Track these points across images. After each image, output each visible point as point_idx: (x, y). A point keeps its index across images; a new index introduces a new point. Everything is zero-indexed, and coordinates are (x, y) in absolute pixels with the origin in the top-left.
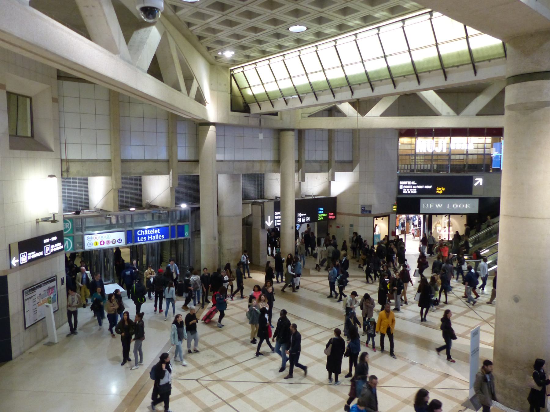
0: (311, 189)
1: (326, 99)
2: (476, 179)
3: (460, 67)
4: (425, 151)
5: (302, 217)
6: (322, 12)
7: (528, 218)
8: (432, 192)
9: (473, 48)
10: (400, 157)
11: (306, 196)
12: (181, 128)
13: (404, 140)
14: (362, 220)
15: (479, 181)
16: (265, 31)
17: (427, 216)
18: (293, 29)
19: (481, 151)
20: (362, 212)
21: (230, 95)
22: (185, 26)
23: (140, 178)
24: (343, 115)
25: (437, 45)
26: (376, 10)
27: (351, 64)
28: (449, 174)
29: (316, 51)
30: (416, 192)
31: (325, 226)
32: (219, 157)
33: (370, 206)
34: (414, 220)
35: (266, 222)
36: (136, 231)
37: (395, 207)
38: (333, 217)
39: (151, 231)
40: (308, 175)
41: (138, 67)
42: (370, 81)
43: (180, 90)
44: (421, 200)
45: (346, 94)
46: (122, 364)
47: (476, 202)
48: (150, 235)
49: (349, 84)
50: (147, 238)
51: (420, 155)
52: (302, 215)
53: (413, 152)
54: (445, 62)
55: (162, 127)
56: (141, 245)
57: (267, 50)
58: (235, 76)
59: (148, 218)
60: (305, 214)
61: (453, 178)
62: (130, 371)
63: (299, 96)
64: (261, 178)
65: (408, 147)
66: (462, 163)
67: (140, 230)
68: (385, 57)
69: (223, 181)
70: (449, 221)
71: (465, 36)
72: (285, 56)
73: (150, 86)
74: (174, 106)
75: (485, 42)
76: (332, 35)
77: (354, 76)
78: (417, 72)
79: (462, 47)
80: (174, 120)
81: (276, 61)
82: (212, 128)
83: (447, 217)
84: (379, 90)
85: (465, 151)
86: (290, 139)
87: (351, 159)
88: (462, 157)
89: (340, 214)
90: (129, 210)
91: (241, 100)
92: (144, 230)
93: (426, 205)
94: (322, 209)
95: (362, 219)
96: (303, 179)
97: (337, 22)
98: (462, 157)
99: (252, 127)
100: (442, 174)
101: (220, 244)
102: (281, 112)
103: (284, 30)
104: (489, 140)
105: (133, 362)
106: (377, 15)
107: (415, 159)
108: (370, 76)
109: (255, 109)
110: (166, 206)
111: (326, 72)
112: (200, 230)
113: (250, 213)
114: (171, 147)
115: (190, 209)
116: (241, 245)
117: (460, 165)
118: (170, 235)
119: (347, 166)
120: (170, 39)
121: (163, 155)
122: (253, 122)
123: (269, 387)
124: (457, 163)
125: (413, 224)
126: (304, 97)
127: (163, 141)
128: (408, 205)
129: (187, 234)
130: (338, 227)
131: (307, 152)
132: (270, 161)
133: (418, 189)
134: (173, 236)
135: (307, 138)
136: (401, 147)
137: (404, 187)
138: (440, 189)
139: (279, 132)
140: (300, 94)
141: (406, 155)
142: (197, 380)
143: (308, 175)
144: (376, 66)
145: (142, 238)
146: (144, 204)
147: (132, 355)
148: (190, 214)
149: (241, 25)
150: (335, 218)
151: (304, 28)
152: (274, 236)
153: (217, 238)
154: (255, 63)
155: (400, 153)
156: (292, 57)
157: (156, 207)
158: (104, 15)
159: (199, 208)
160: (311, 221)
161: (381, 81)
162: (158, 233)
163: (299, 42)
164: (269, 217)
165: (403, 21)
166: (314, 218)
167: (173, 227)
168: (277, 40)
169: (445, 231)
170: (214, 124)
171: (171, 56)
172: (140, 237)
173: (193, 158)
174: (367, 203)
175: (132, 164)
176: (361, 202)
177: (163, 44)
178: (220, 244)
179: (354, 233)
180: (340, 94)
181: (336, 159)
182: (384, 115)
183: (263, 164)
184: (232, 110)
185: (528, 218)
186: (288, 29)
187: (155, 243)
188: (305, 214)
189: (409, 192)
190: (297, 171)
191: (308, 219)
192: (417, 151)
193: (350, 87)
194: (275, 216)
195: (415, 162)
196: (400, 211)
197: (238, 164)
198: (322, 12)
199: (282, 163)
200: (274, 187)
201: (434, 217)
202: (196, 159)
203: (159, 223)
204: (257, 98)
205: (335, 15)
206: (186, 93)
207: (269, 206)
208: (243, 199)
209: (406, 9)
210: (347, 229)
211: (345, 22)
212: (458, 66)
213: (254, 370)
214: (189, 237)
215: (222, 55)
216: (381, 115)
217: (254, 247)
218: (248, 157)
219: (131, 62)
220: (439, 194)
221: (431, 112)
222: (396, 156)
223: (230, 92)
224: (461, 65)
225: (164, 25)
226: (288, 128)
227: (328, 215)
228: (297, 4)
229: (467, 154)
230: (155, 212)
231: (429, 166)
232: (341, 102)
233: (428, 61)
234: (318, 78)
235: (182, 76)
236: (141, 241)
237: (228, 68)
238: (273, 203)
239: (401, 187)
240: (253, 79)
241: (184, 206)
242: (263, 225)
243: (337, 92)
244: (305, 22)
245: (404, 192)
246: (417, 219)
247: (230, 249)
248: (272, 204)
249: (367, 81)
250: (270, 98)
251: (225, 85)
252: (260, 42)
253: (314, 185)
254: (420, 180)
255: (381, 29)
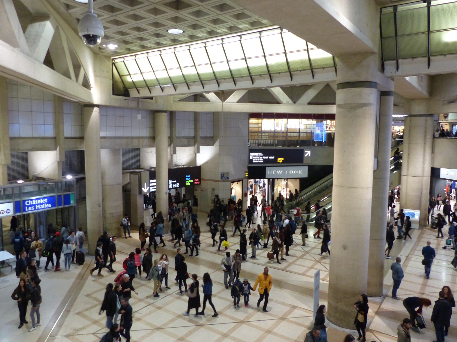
0: (180, 160)
1: (195, 89)
2: (306, 152)
3: (302, 72)
4: (269, 130)
5: (173, 183)
6: (198, 21)
7: (352, 187)
8: (274, 161)
9: (312, 58)
10: (250, 134)
11: (176, 165)
12: (67, 109)
13: (253, 121)
14: (222, 184)
15: (308, 153)
16: (147, 31)
17: (271, 180)
18: (171, 31)
19: (309, 130)
20: (222, 178)
21: (111, 81)
22: (75, 21)
23: (26, 154)
24: (207, 100)
25: (285, 53)
26: (240, 23)
27: (218, 63)
28: (285, 147)
29: (189, 50)
30: (262, 162)
31: (191, 189)
32: (103, 134)
33: (228, 173)
34: (260, 183)
35: (143, 189)
36: (24, 201)
37: (247, 173)
38: (198, 183)
39: (39, 201)
40: (178, 149)
41: (35, 59)
42: (233, 77)
43: (69, 77)
44: (267, 168)
45: (214, 87)
46: (20, 327)
47: (306, 168)
48: (38, 204)
49: (217, 79)
50: (35, 207)
51: (265, 132)
52: (173, 181)
53: (260, 130)
54: (291, 67)
55: (49, 108)
56: (28, 215)
57: (147, 45)
58: (116, 64)
59: (35, 189)
60: (176, 181)
61: (288, 150)
62: (28, 333)
63: (173, 85)
64: (137, 152)
65: (256, 126)
66: (295, 139)
67: (28, 200)
68: (245, 59)
69: (105, 156)
70: (287, 183)
71: (306, 48)
72: (162, 51)
73: (45, 76)
74: (66, 92)
75: (320, 55)
76: (203, 38)
77: (220, 72)
78: (270, 73)
79: (303, 56)
80: (59, 101)
81: (154, 55)
82: (96, 109)
83: (286, 180)
84: (240, 84)
85: (298, 130)
86: (164, 119)
87: (212, 136)
88: (295, 134)
89: (204, 180)
90: (17, 183)
91: (121, 85)
92: (32, 200)
93: (271, 172)
94: (189, 176)
95: (222, 184)
96: (174, 152)
97: (208, 29)
98: (295, 134)
99: (131, 109)
100: (280, 147)
101: (104, 211)
102: (156, 97)
103: (164, 32)
104: (314, 121)
105: (30, 324)
106: (240, 26)
107: (261, 136)
108: (233, 73)
109: (133, 93)
110: (51, 178)
111: (197, 67)
112: (85, 198)
113: (129, 181)
114: (58, 125)
115: (75, 179)
116: (122, 210)
117: (294, 141)
118: (57, 204)
119: (209, 141)
120: (62, 32)
121: (49, 131)
122: (132, 104)
123: (158, 332)
124: (292, 139)
125: (259, 186)
126: (178, 86)
127: (50, 119)
128: (257, 172)
129: (72, 202)
130: (202, 191)
131: (177, 130)
132: (146, 138)
133: (264, 159)
134: (60, 204)
135: (177, 118)
136: (251, 126)
137: (254, 157)
138: (280, 159)
139: (154, 113)
140: (174, 84)
141: (254, 132)
142: (94, 334)
143: (178, 149)
144: (238, 66)
145: (30, 208)
146: (30, 176)
147: (28, 317)
148: (75, 183)
149: (127, 25)
150: (200, 184)
151: (181, 31)
152: (151, 200)
153: (101, 205)
154: (135, 55)
155: (250, 131)
156: (168, 52)
157: (43, 179)
158: (6, 12)
159: (84, 178)
160: (181, 186)
161: (242, 77)
162: (45, 203)
163: (175, 41)
164: (145, 184)
165: (260, 32)
166: (183, 184)
167: (59, 197)
168: (157, 39)
169: (284, 192)
170: (97, 106)
171: (63, 48)
172: (28, 206)
173: (78, 135)
174: (225, 171)
175: (21, 141)
176: (221, 170)
177: (56, 38)
178: (104, 211)
179: (216, 195)
180: (208, 85)
181: (201, 135)
182: (240, 101)
183: (141, 140)
184: (114, 94)
185: (352, 187)
186: (167, 31)
187: (42, 212)
188: (176, 181)
189: (257, 162)
190: (170, 145)
191: (178, 185)
192: (263, 129)
193: (217, 81)
194: (150, 183)
195: (261, 138)
196: (250, 177)
197: (118, 140)
198: (198, 21)
199: (157, 140)
200: (150, 158)
201: (276, 181)
202: (81, 136)
203: (46, 193)
204: (136, 85)
205: (208, 23)
206: (75, 80)
207: (145, 175)
208: (124, 169)
209: (263, 24)
210: (209, 192)
211: (215, 29)
212: (301, 71)
213: (144, 319)
214: (74, 205)
215: (106, 47)
216: (238, 102)
217: (132, 211)
218: (128, 134)
219: (30, 55)
220: (279, 163)
221: (275, 101)
222: (247, 133)
223: (111, 78)
224: (303, 70)
225: (56, 20)
226: (162, 110)
227: (194, 181)
228: (178, 13)
229: (299, 133)
230: (42, 184)
231: (272, 141)
232: (208, 92)
233: (279, 65)
234: (190, 72)
235: (72, 66)
236: (29, 210)
237: (110, 57)
238: (148, 172)
239: (251, 158)
240: (133, 69)
241: (69, 177)
242: (140, 191)
243: (205, 84)
244: (183, 27)
245: (253, 162)
246: (262, 182)
247: (112, 214)
248: (148, 173)
249: (231, 77)
250: (147, 85)
251: (108, 72)
252: (141, 39)
253: (183, 157)
254: (265, 152)
255: (243, 37)
